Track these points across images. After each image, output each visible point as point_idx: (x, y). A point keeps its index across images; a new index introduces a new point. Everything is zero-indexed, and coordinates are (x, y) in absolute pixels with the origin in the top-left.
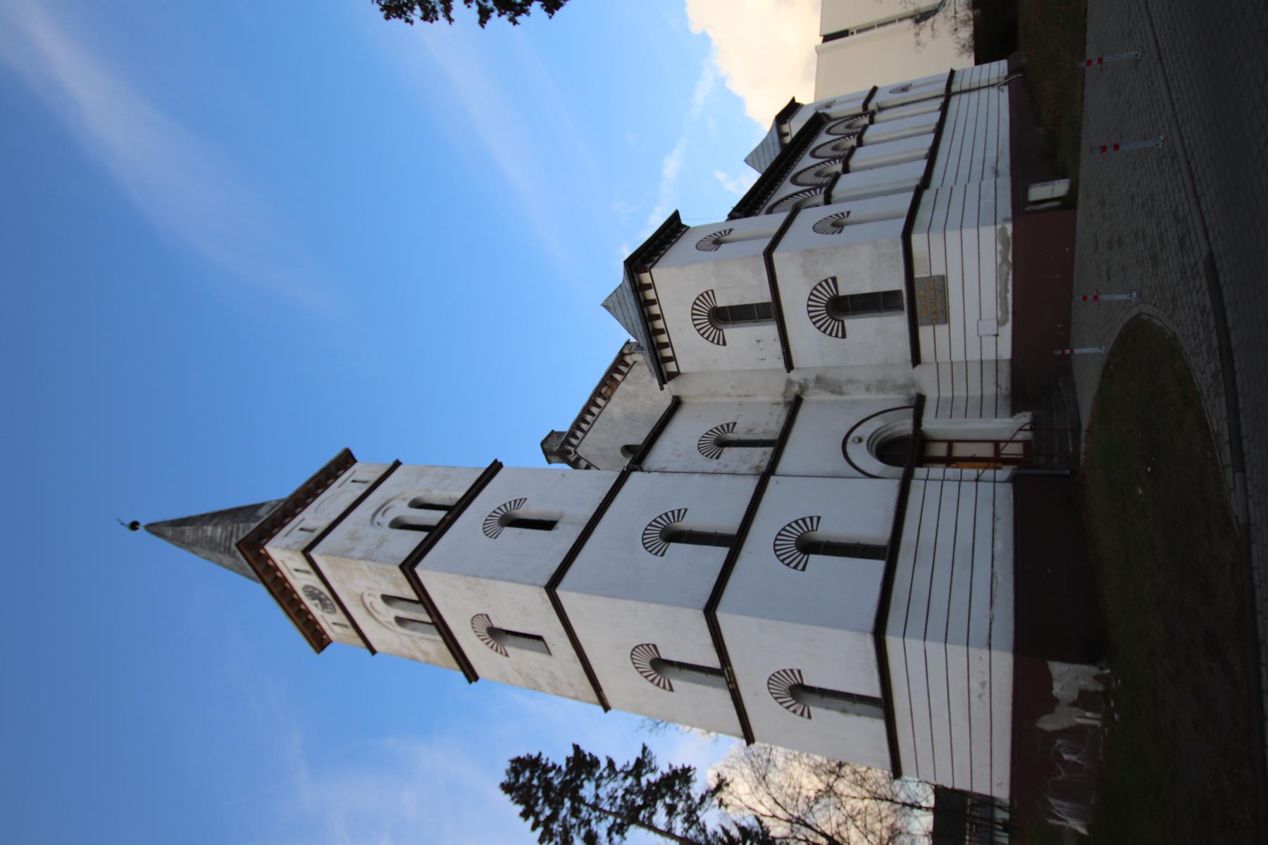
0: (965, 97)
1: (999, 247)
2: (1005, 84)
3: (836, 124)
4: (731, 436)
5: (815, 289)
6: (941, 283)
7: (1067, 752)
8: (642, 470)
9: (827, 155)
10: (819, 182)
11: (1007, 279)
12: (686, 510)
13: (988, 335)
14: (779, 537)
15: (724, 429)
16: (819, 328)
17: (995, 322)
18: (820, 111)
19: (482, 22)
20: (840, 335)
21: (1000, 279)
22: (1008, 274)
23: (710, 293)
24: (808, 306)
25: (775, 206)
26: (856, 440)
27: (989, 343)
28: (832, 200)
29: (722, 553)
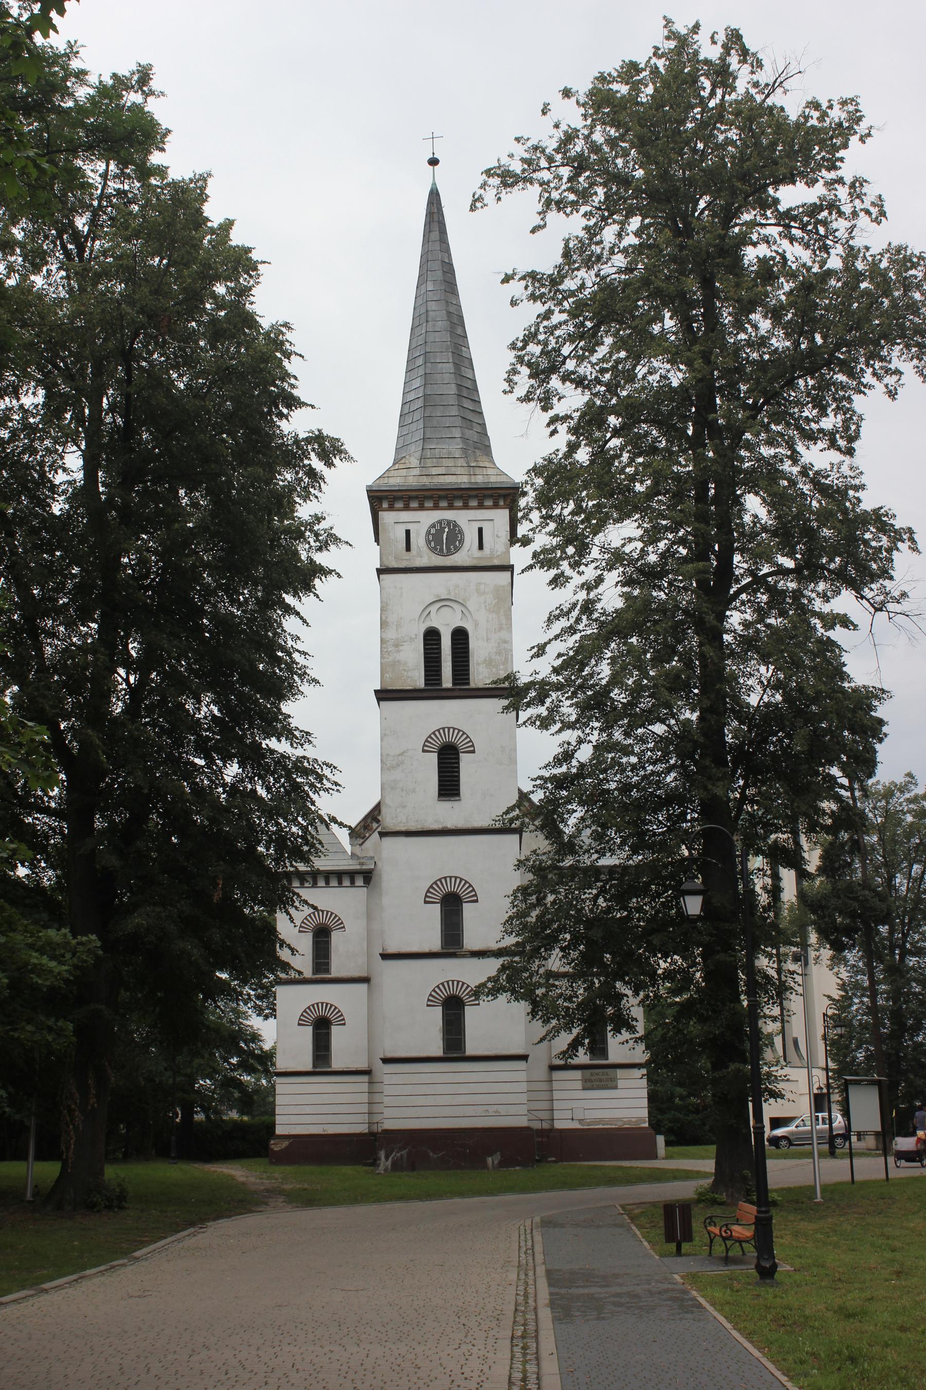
6: (611, 1085)
27: (568, 1115)
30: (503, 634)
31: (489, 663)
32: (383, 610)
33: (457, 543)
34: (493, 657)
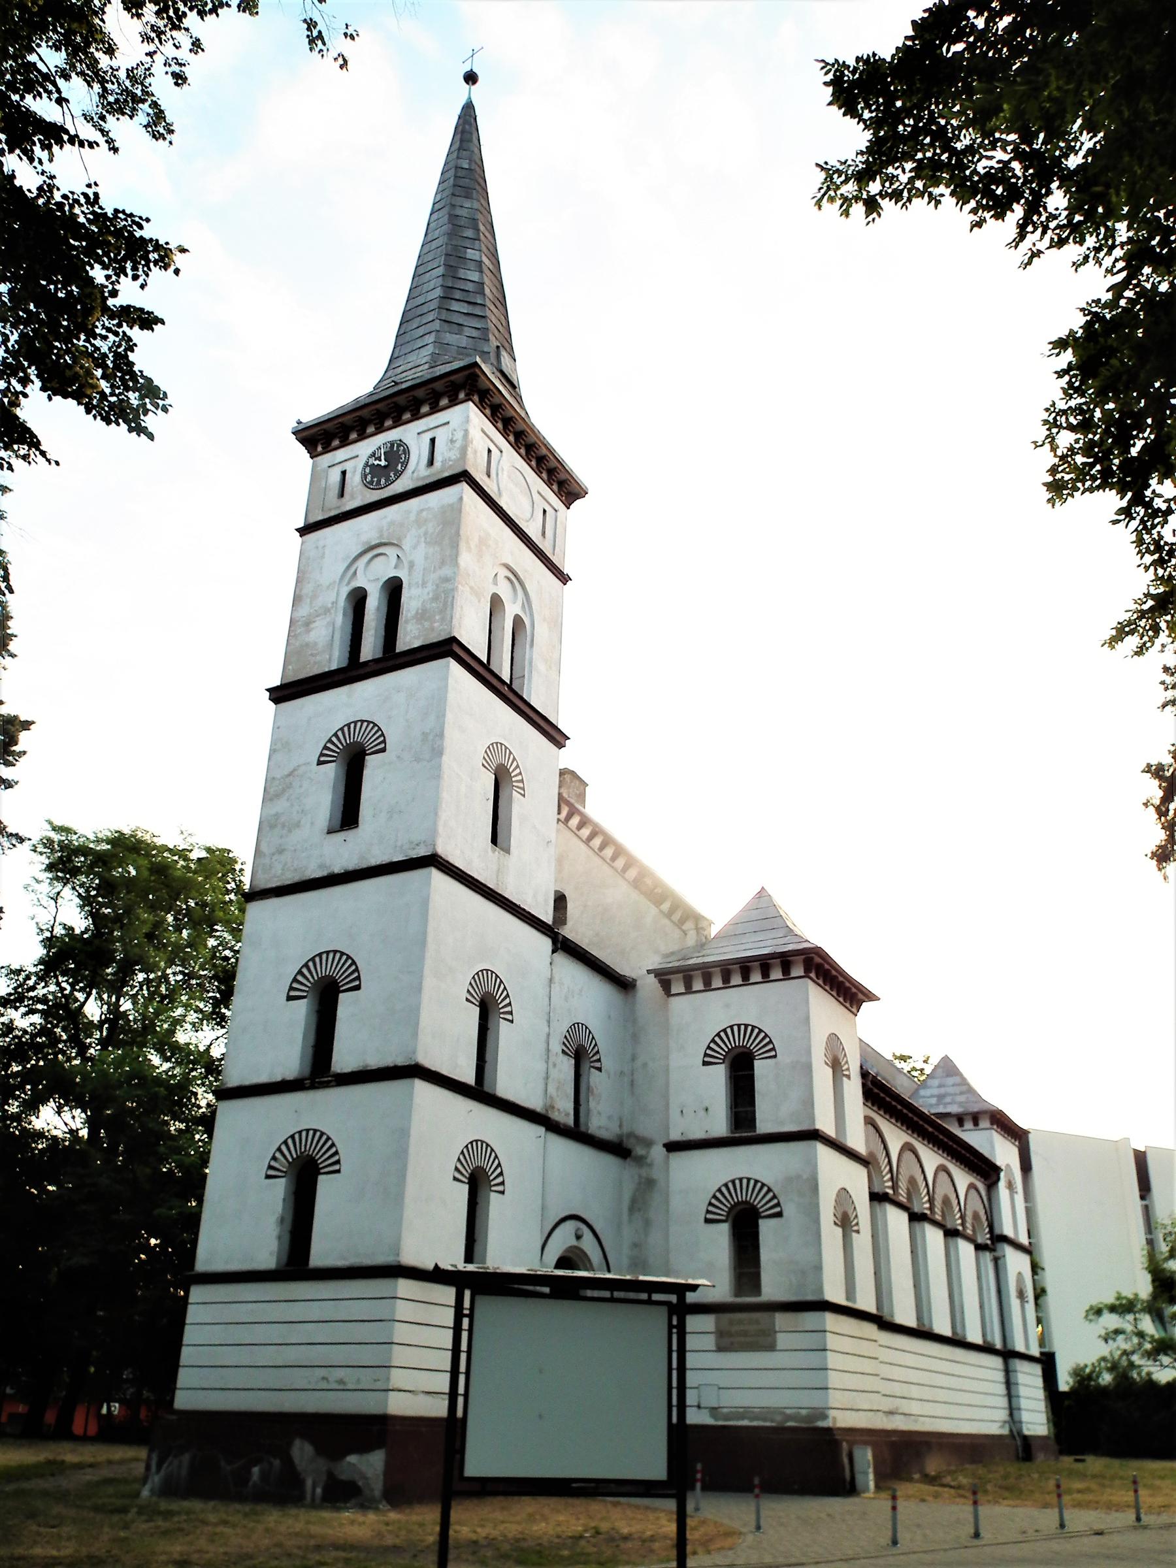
0: (1000, 1376)
1: (804, 1412)
2: (1011, 1431)
3: (981, 1197)
4: (585, 1067)
5: (769, 1190)
6: (764, 1342)
7: (262, 1472)
8: (554, 952)
9: (937, 1190)
10: (900, 1184)
11: (765, 1420)
12: (512, 1021)
13: (699, 1397)
14: (484, 1145)
15: (595, 1061)
16: (719, 1190)
17: (716, 1406)
18: (1002, 1175)
19: (1143, 771)
20: (710, 1216)
21: (767, 1412)
22: (772, 1421)
23: (773, 1053)
24: (749, 1180)
25: (874, 1127)
26: (580, 1233)
28: (876, 1203)
29: (468, 1076)
30: (446, 571)
31: (422, 615)
32: (299, 581)
33: (399, 467)
34: (428, 606)
